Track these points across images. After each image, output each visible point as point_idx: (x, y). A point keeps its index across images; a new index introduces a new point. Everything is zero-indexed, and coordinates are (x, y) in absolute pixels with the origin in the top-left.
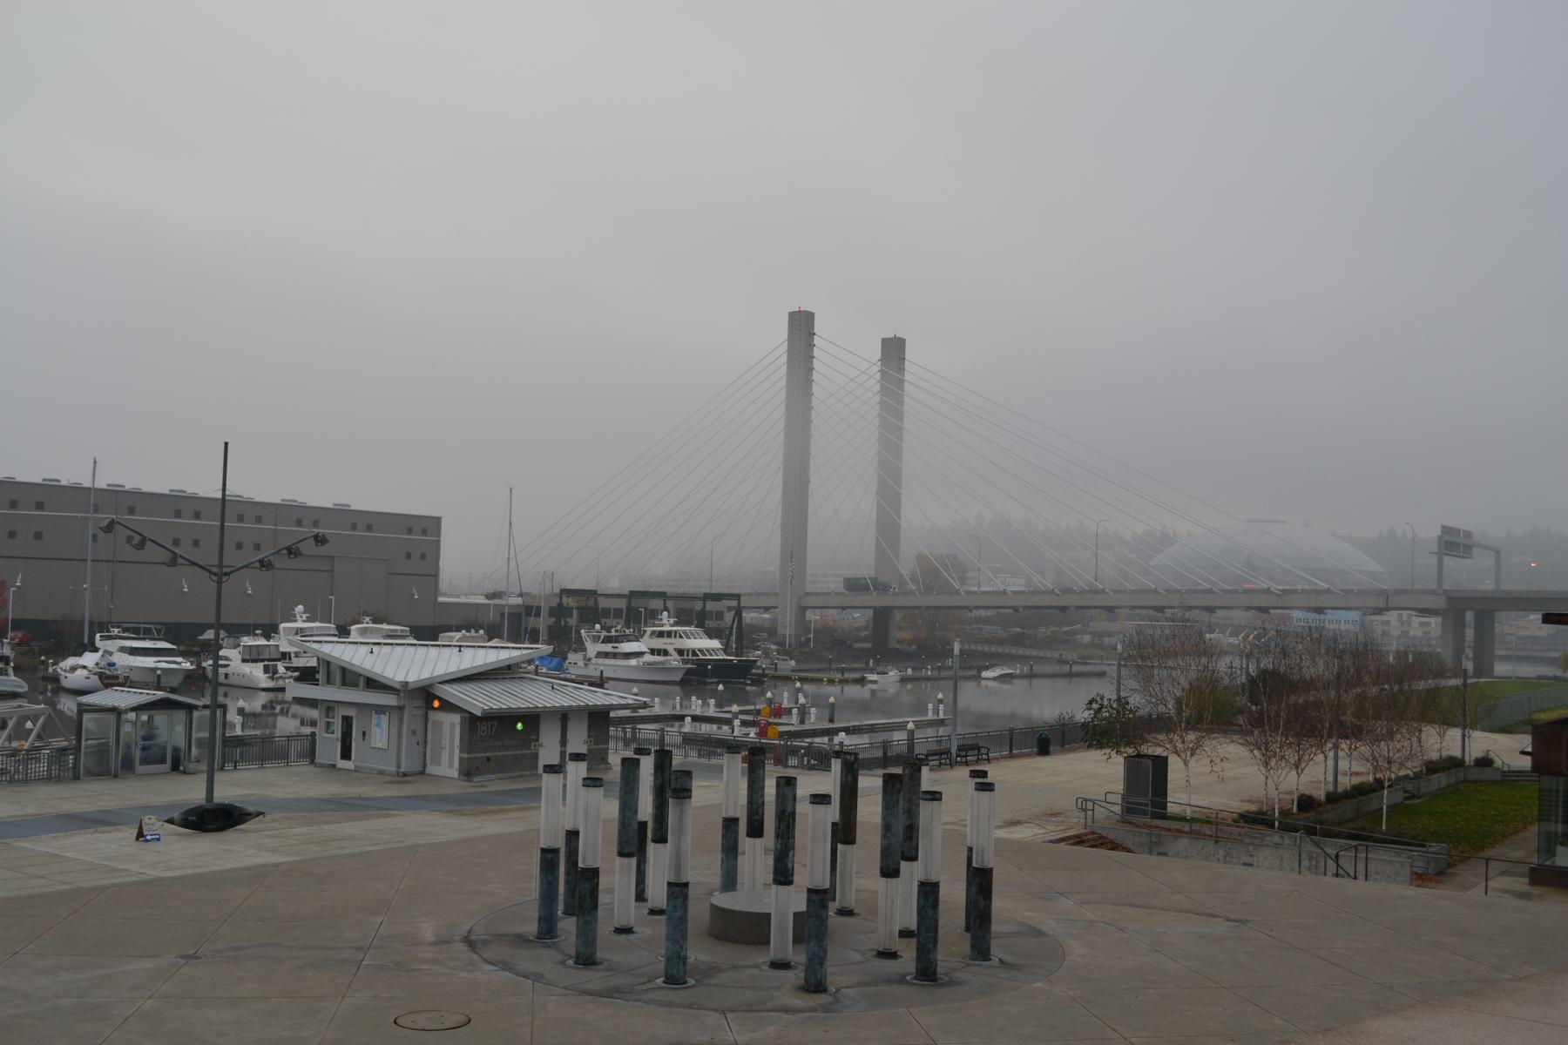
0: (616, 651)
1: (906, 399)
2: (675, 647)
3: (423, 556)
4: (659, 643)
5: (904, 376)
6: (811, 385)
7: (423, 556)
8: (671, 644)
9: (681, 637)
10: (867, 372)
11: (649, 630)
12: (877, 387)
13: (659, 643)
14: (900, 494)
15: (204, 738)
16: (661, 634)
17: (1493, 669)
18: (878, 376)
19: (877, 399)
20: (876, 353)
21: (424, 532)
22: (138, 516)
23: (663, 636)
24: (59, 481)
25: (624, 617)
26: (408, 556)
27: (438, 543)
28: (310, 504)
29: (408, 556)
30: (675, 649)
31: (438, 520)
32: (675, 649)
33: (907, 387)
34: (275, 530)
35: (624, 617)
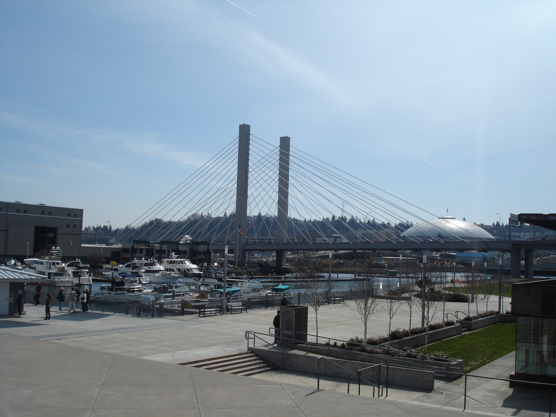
0: (150, 269)
1: (290, 163)
2: (177, 267)
3: (75, 226)
4: (170, 266)
5: (289, 153)
6: (249, 155)
7: (75, 226)
8: (175, 267)
9: (179, 263)
10: (271, 151)
11: (166, 260)
12: (278, 158)
13: (170, 266)
14: (288, 203)
15: (509, 258)
16: (171, 262)
17: (513, 392)
18: (279, 153)
19: (278, 162)
20: (278, 143)
21: (75, 216)
22: (71, 217)
23: (172, 263)
24: (45, 205)
25: (130, 252)
26: (68, 226)
27: (82, 221)
28: (47, 205)
29: (68, 226)
30: (176, 269)
31: (81, 211)
32: (176, 269)
33: (291, 157)
34: (7, 214)
35: (130, 252)
